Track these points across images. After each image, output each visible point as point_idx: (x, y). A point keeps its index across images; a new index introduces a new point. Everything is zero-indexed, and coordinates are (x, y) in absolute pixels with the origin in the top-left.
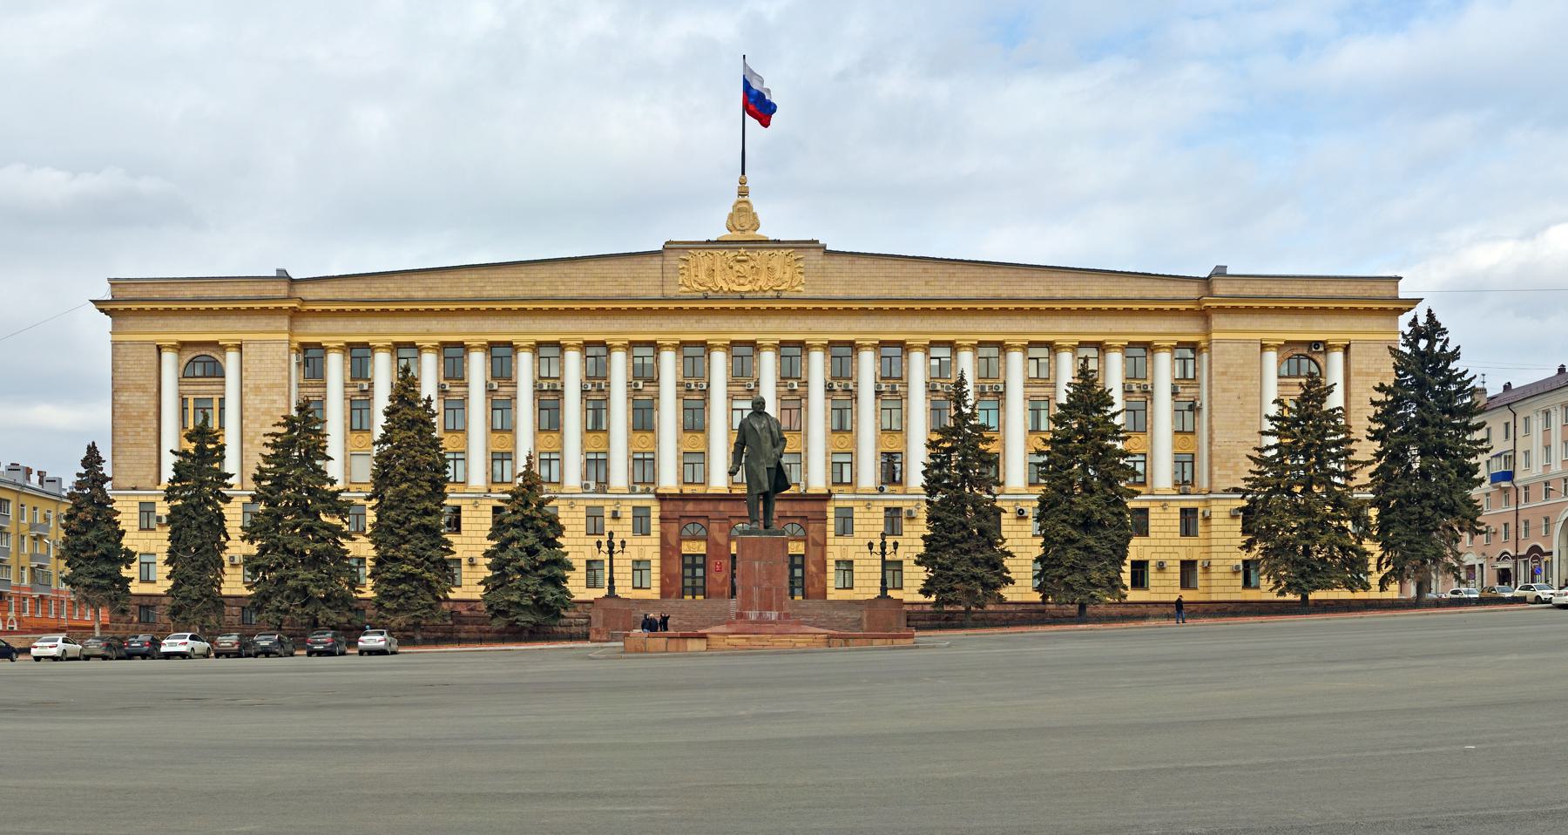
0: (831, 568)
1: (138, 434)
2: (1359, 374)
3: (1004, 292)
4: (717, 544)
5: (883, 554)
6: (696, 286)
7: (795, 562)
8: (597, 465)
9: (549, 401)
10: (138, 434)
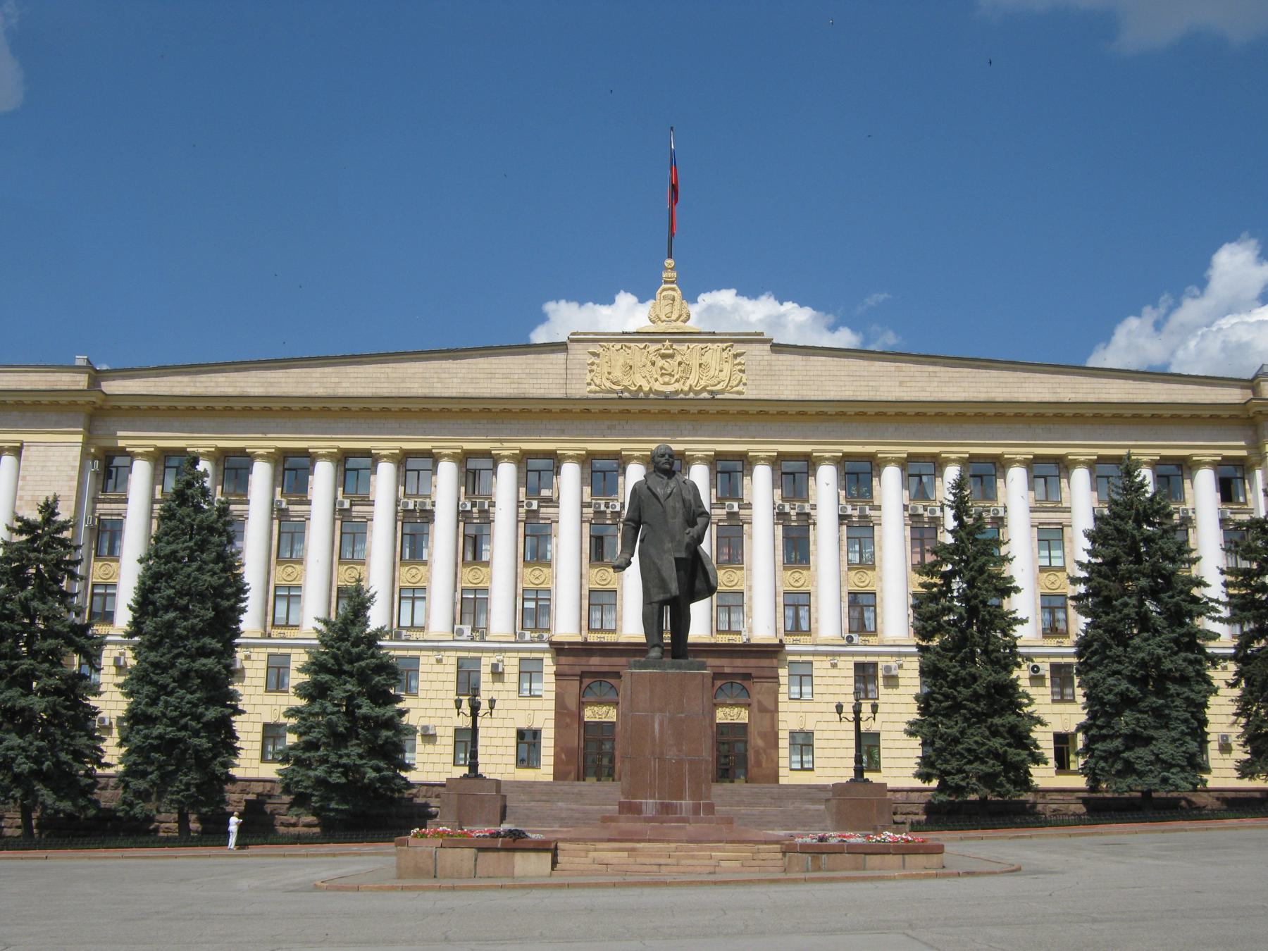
0: (784, 743)
3: (1000, 394)
5: (857, 720)
6: (608, 384)
7: (731, 737)
8: (471, 606)
9: (413, 526)
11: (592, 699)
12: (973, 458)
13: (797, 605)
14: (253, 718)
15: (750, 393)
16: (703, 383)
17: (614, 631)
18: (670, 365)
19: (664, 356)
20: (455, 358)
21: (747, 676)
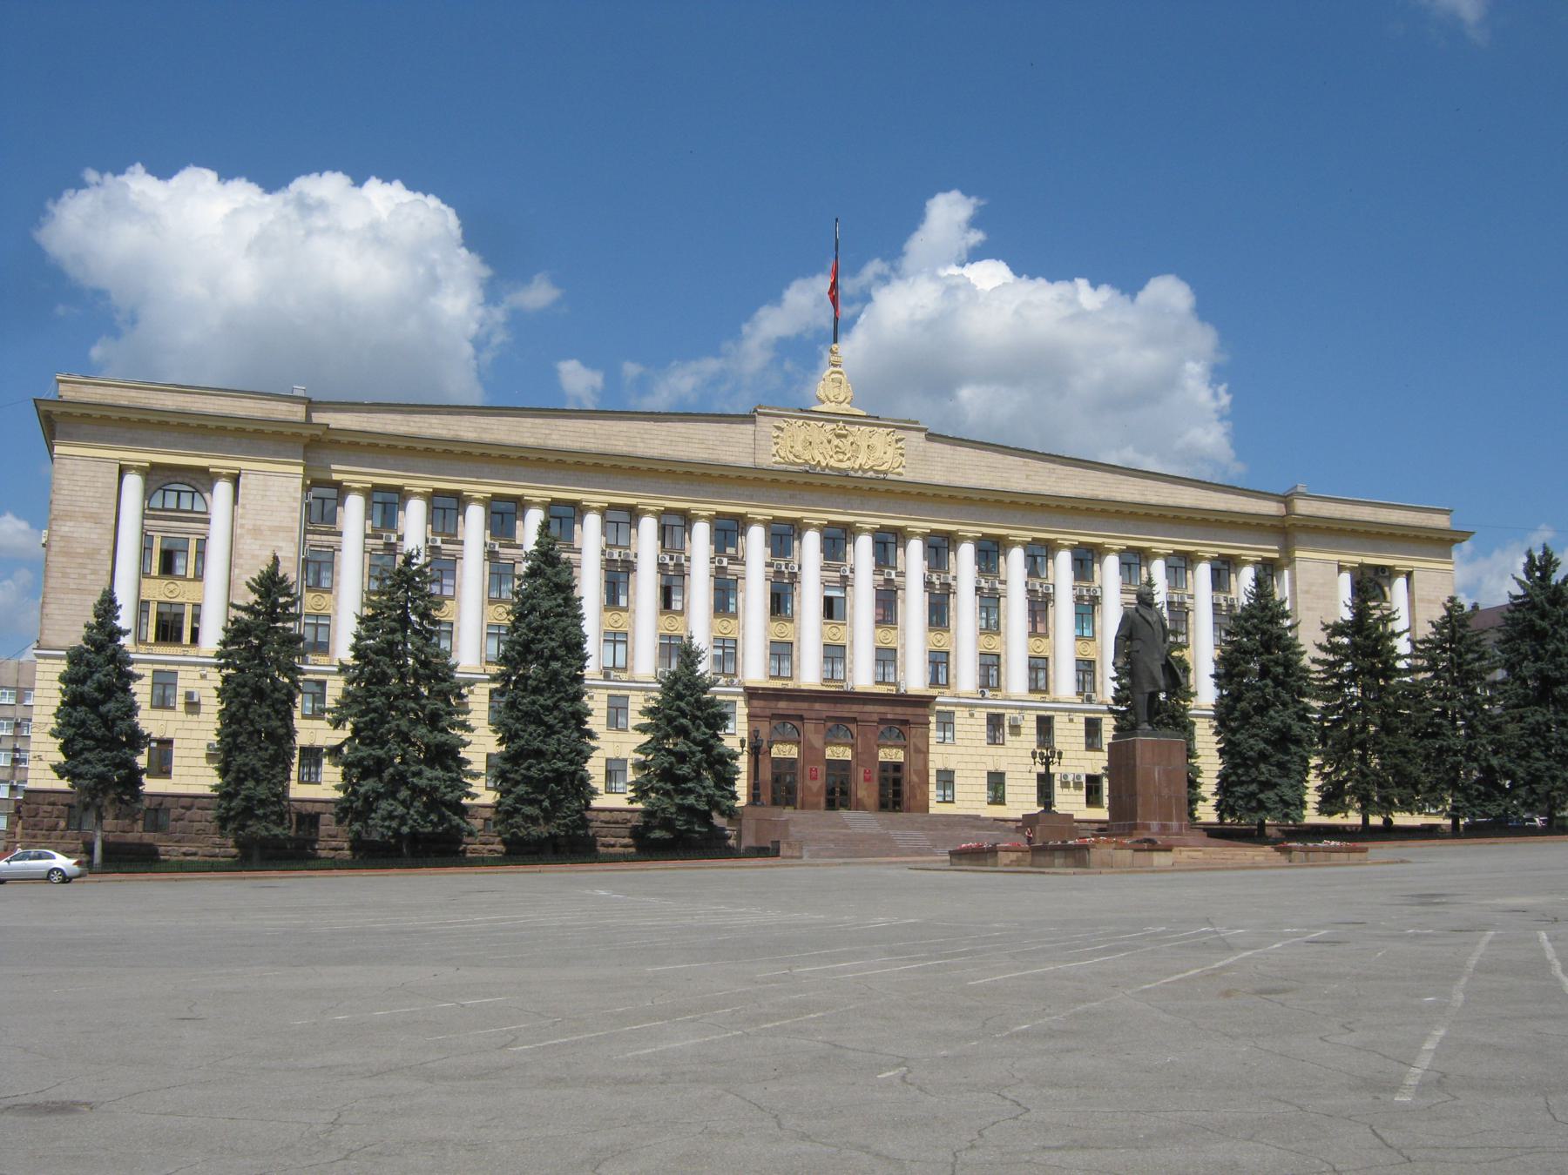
0: (933, 779)
1: (84, 577)
2: (1422, 600)
4: (812, 748)
6: (791, 457)
8: (990, 666)
10: (84, 577)
11: (779, 738)
12: (556, 502)
13: (939, 662)
14: (477, 748)
15: (908, 476)
16: (871, 463)
17: (791, 678)
18: (845, 444)
19: (839, 436)
20: (656, 421)
21: (905, 722)
